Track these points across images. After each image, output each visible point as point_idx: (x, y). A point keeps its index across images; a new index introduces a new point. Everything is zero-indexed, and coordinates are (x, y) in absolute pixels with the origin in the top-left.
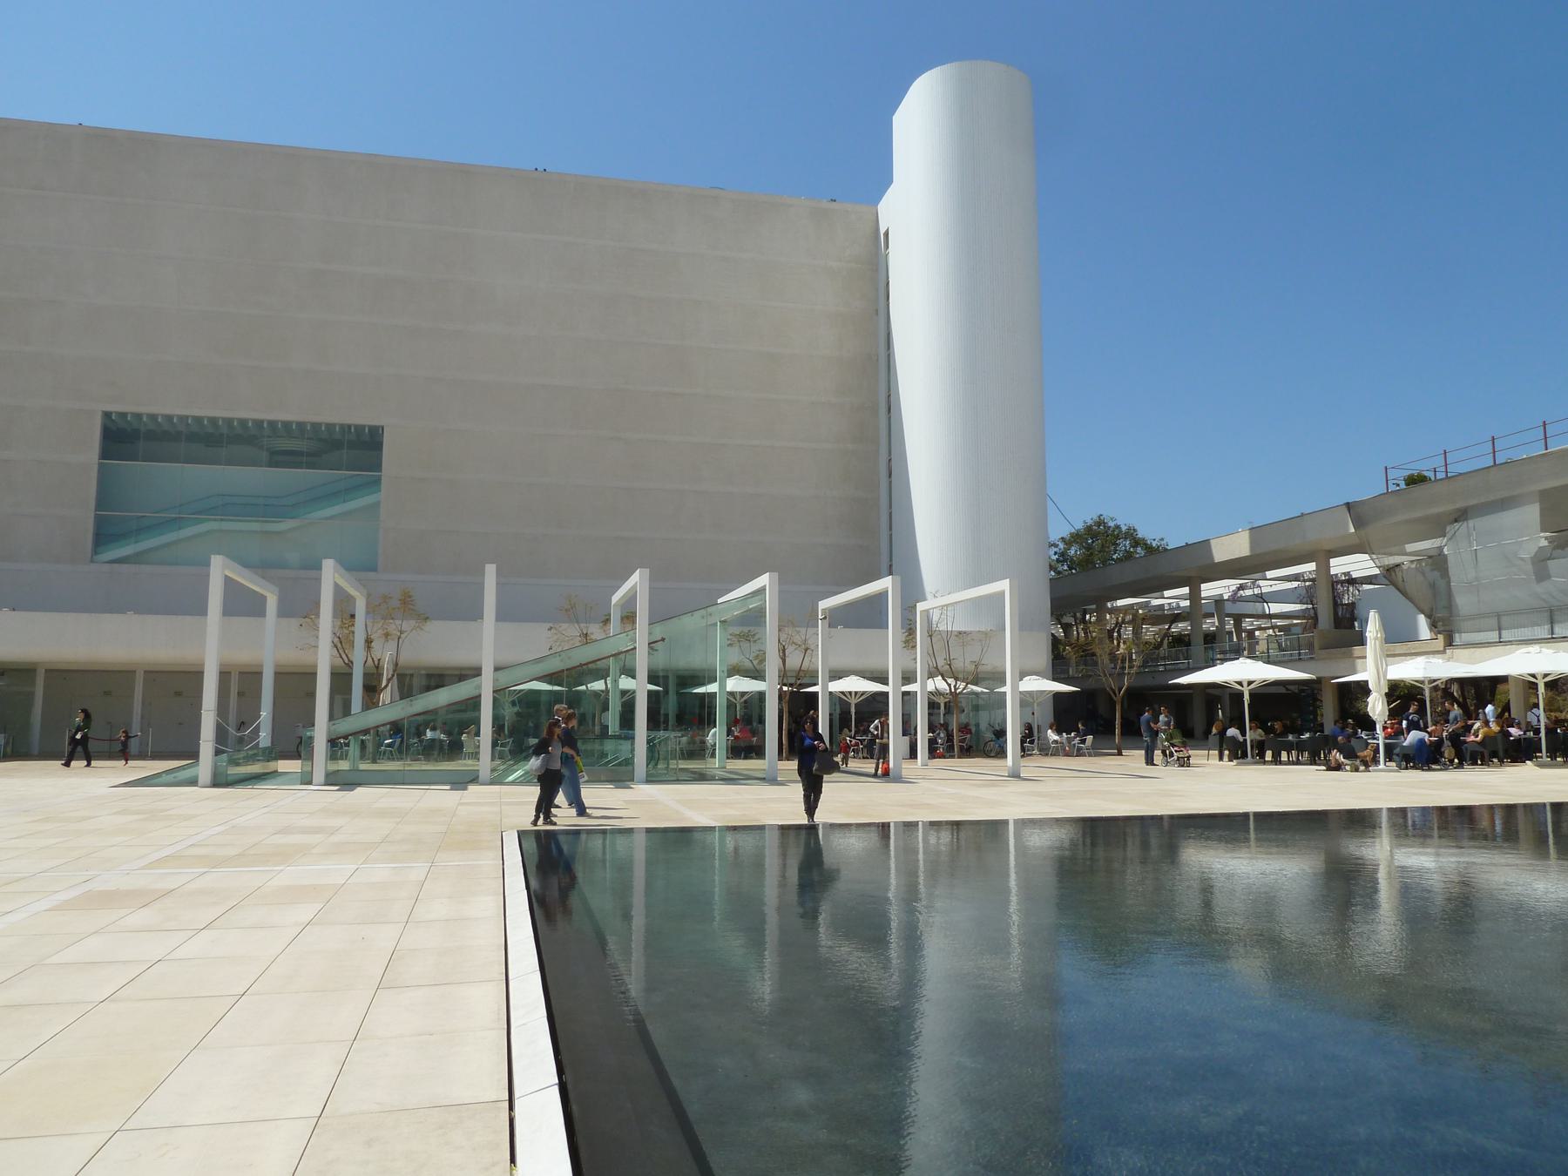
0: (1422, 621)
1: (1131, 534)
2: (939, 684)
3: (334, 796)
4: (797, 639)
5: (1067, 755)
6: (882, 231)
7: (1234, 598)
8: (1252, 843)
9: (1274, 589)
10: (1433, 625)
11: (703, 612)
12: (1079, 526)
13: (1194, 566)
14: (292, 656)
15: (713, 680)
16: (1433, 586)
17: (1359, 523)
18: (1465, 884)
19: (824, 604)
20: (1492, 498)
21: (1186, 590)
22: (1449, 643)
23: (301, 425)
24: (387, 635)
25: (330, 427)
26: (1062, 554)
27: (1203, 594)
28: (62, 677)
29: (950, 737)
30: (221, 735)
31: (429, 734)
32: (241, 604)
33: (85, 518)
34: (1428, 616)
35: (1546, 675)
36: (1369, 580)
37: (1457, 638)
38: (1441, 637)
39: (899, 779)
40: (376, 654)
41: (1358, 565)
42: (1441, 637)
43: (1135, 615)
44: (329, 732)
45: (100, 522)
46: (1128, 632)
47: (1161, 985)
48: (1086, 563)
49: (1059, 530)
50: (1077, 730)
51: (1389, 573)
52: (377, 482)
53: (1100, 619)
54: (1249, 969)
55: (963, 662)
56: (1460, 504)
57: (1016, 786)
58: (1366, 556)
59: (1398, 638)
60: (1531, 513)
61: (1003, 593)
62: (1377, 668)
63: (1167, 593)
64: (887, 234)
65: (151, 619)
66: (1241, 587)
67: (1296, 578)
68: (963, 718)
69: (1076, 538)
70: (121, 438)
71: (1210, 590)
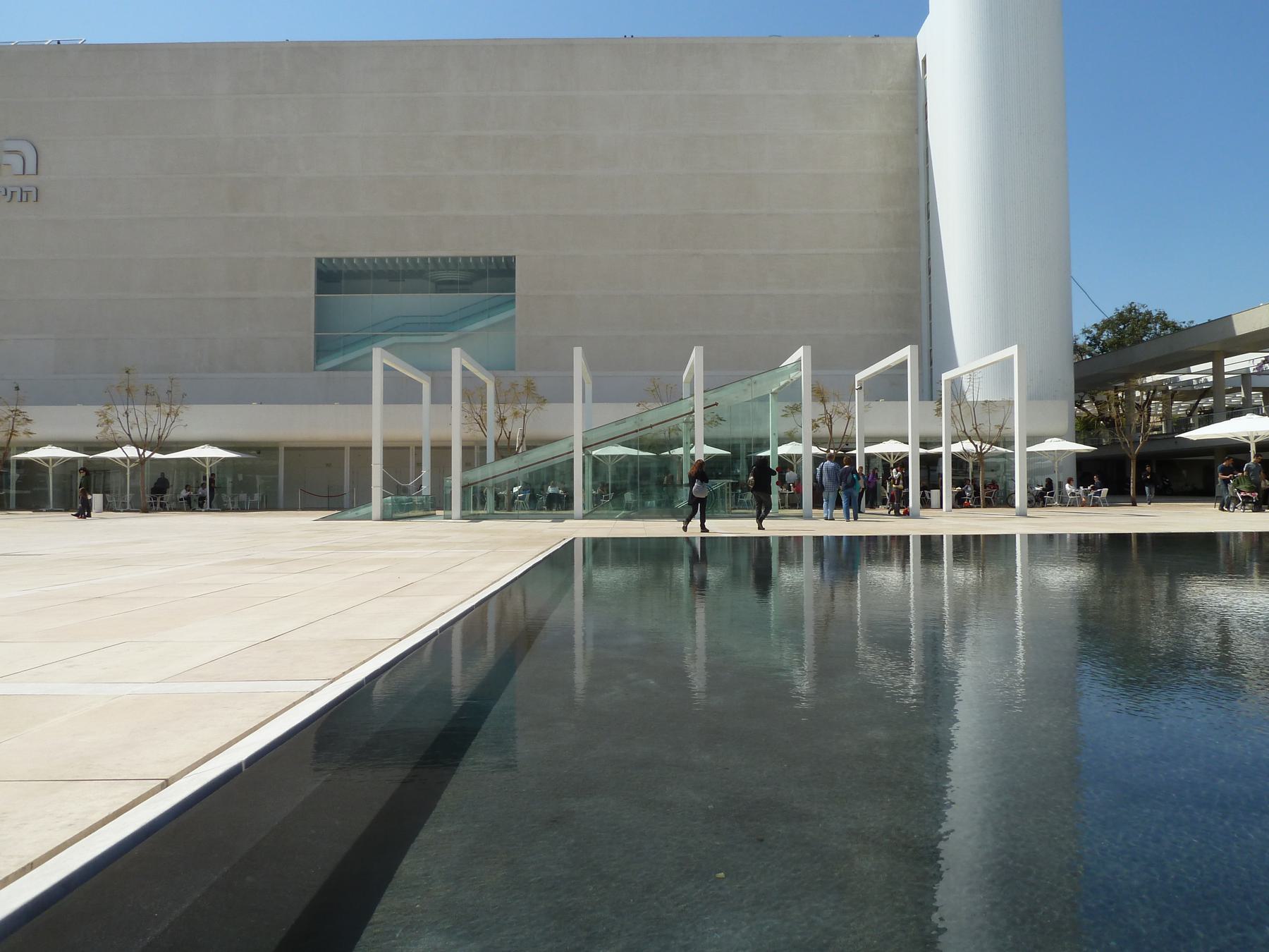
1: (1161, 318)
2: (968, 446)
4: (842, 409)
5: (1083, 505)
11: (748, 381)
14: (439, 433)
15: (767, 447)
19: (860, 376)
21: (1209, 365)
23: (455, 259)
24: (516, 414)
25: (476, 259)
27: (1227, 369)
28: (298, 452)
29: (977, 493)
30: (387, 484)
31: (550, 490)
32: (400, 392)
39: (917, 517)
40: (508, 428)
43: (1166, 391)
45: (319, 342)
46: (1157, 407)
47: (1183, 715)
48: (1118, 344)
49: (1088, 316)
52: (512, 301)
53: (1129, 393)
55: (988, 429)
57: (1024, 520)
63: (1194, 368)
65: (350, 408)
68: (991, 476)
69: (1108, 324)
70: (330, 277)
71: (1234, 364)
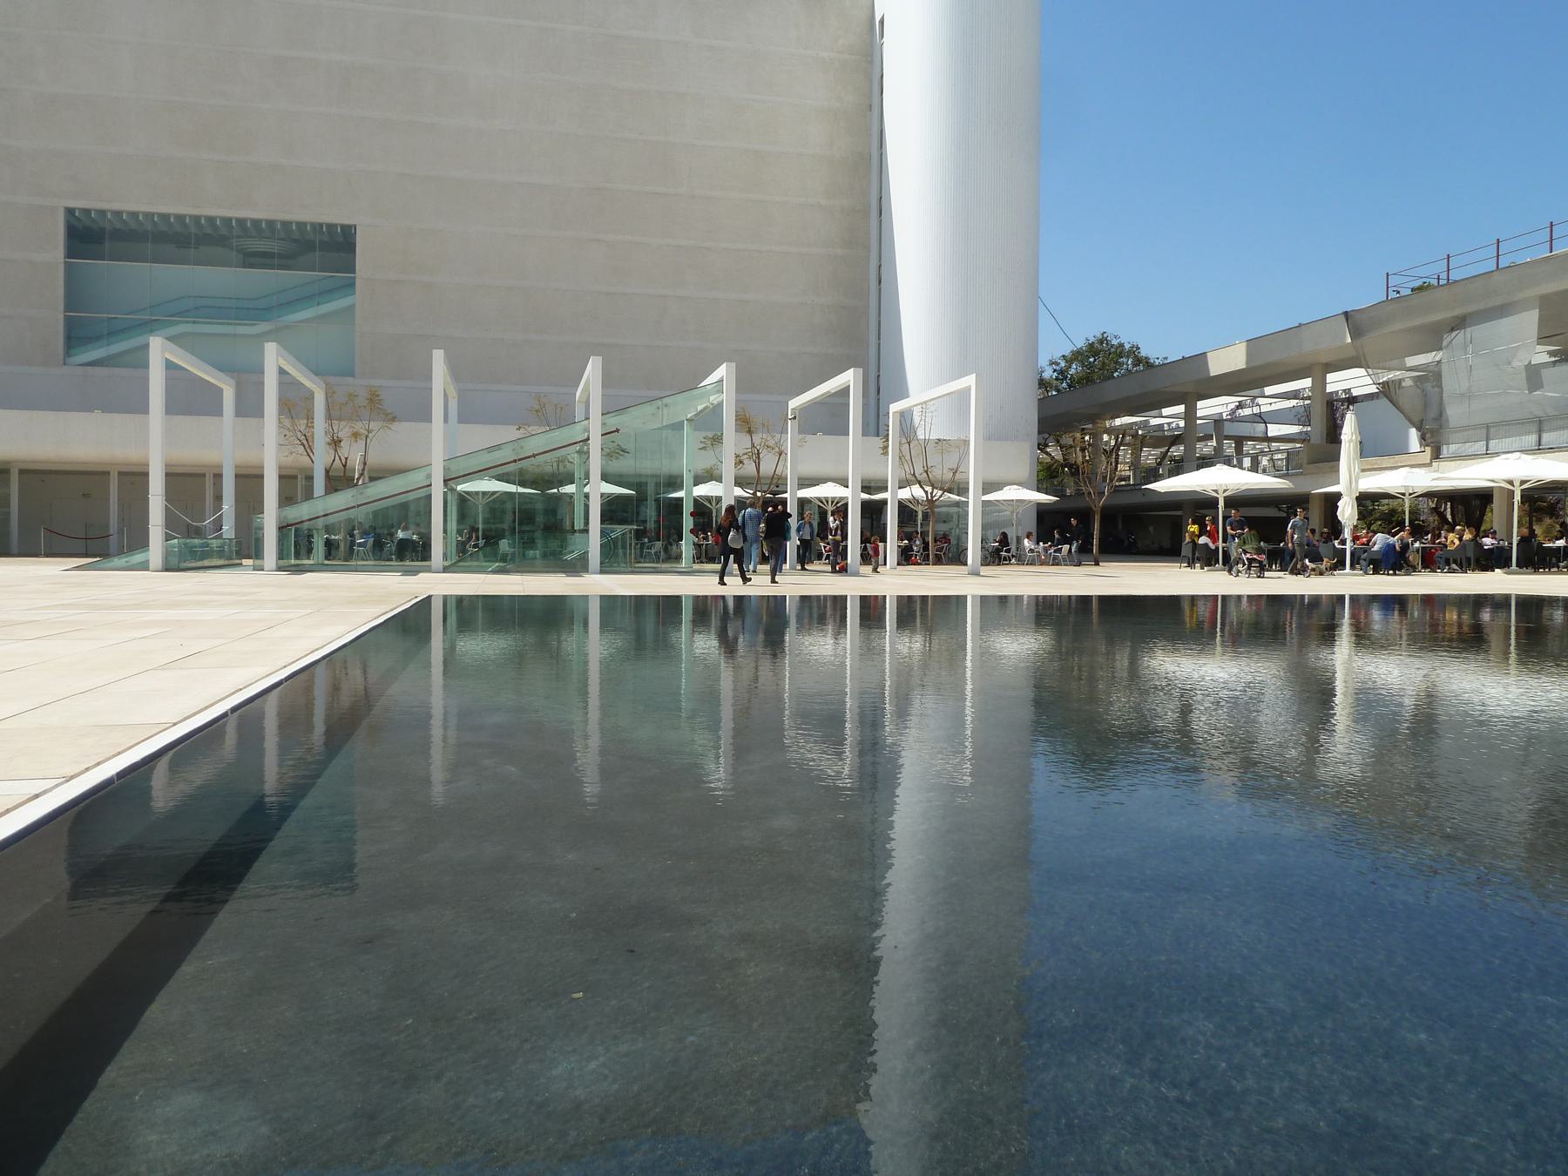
0: (1413, 434)
1: (1134, 352)
3: (284, 577)
4: (771, 443)
5: (1043, 563)
6: (878, 19)
7: (1234, 418)
8: (1219, 649)
9: (1274, 407)
10: (1423, 438)
12: (1080, 343)
13: (1190, 382)
16: (1425, 394)
17: (1356, 333)
18: (1429, 696)
19: (795, 403)
20: (1491, 304)
21: (1181, 409)
22: (1437, 455)
23: (271, 223)
26: (1062, 372)
29: (926, 547)
33: (56, 319)
34: (1419, 429)
35: (1522, 482)
36: (1370, 397)
37: (1445, 451)
38: (1428, 449)
41: (1355, 381)
42: (1428, 449)
43: (1135, 436)
44: (279, 518)
46: (1125, 454)
47: (1144, 801)
48: (1086, 380)
49: (1057, 344)
50: (1052, 539)
51: (1387, 391)
54: (1221, 780)
55: (941, 472)
56: (1457, 312)
58: (1362, 371)
59: (1375, 449)
60: (1529, 320)
61: (969, 388)
62: (1353, 479)
63: (1166, 411)
64: (882, 22)
66: (1240, 406)
67: (1295, 395)
68: (943, 528)
69: (1077, 356)
70: (87, 236)
71: (1208, 408)
